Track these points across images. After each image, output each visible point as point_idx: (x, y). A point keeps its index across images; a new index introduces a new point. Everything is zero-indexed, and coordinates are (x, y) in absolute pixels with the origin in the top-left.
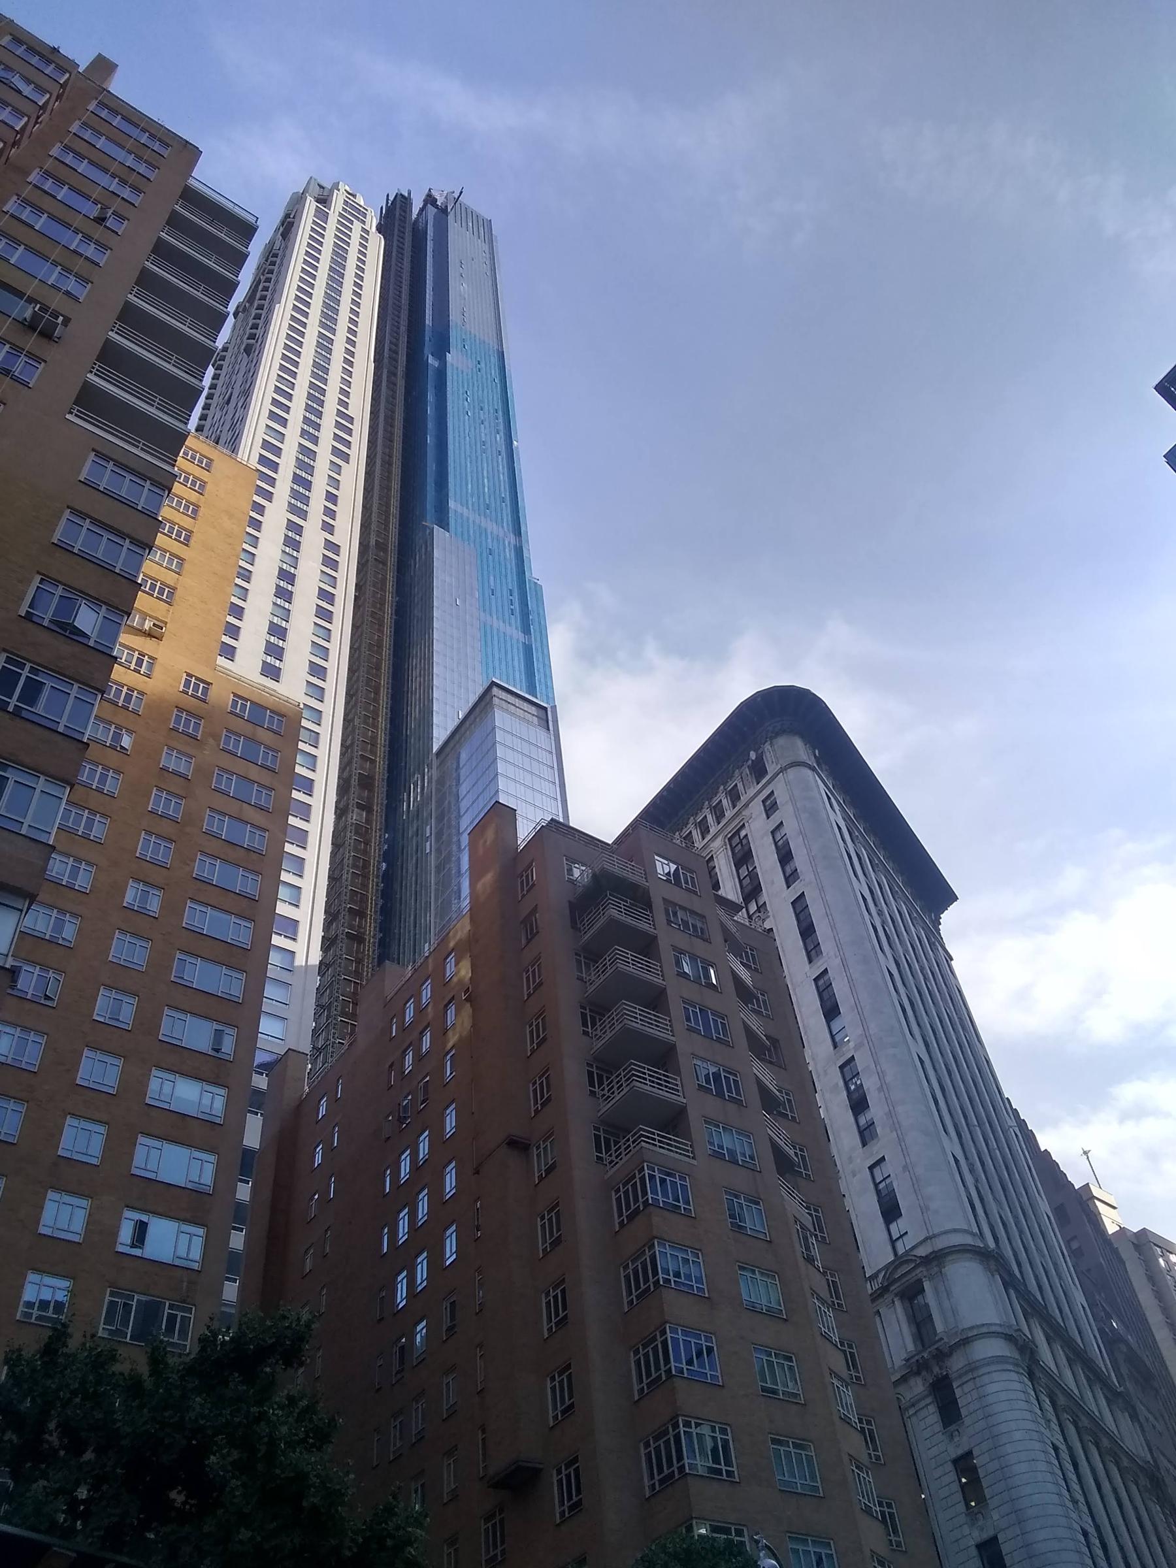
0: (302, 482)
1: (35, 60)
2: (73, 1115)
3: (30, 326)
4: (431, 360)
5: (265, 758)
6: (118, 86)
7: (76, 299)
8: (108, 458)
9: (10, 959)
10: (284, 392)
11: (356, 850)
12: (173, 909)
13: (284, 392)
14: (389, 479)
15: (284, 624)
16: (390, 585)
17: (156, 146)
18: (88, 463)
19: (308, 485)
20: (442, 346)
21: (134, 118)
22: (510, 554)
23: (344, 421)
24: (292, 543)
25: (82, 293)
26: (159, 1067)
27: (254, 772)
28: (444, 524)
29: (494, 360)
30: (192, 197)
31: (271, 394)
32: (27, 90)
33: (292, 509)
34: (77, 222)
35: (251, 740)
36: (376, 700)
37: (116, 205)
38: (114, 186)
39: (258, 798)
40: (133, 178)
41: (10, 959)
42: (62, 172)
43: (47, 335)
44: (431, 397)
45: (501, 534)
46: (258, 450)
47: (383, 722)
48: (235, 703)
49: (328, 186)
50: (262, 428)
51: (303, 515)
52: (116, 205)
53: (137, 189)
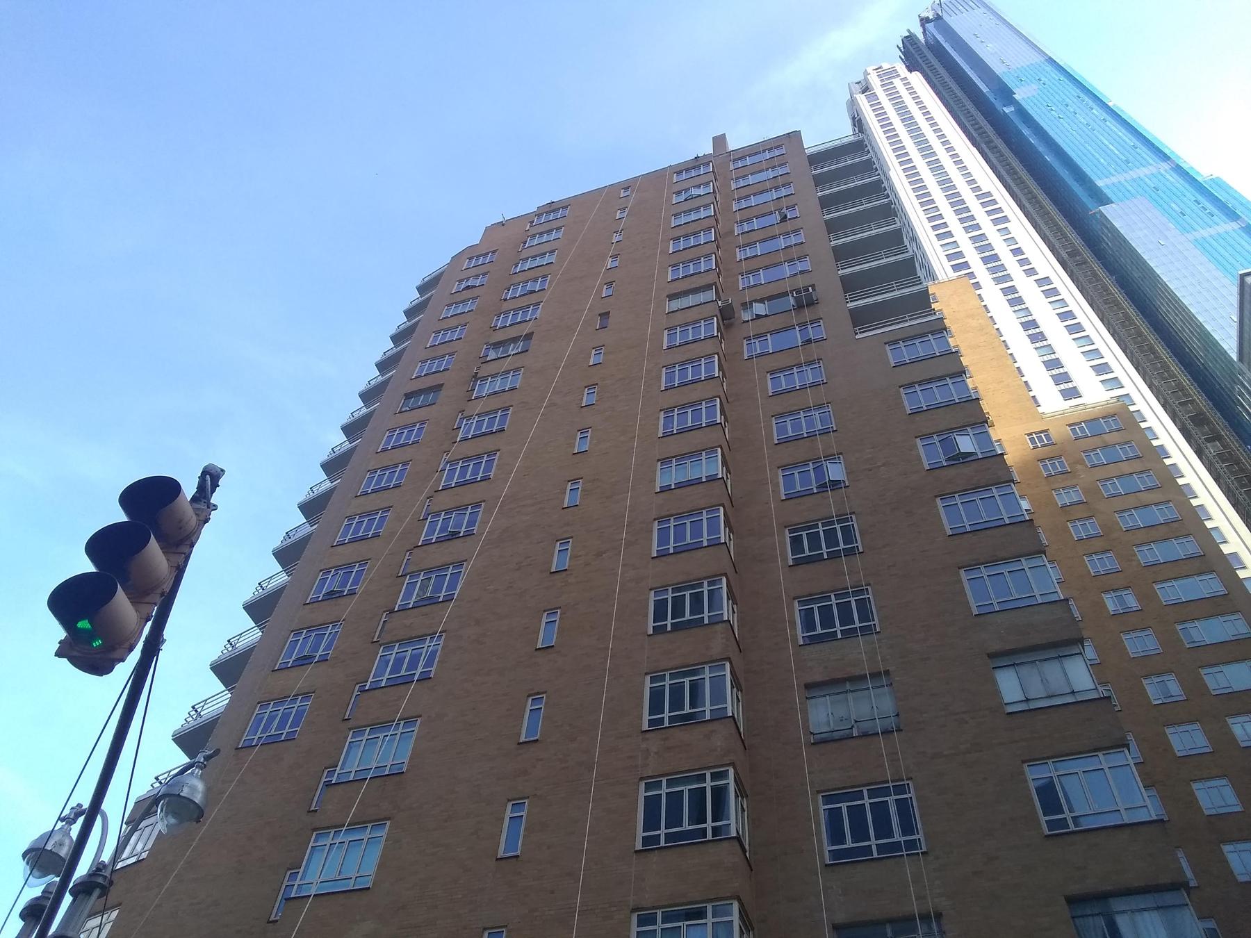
0: (991, 259)
1: (693, 173)
2: (1195, 780)
3: (799, 306)
4: (1007, 110)
5: (1125, 453)
6: (733, 144)
7: (808, 271)
8: (897, 342)
9: (1100, 689)
10: (935, 218)
11: (1233, 473)
12: (1147, 597)
13: (935, 218)
14: (1042, 207)
15: (1053, 357)
16: (1101, 273)
17: (776, 153)
18: (889, 353)
19: (995, 257)
20: (1006, 94)
21: (753, 151)
22: (1173, 178)
23: (986, 200)
24: (1016, 302)
25: (806, 265)
26: (1232, 715)
27: (1126, 468)
28: (1104, 200)
29: (1049, 68)
30: (817, 159)
31: (928, 225)
32: (701, 191)
33: (998, 280)
34: (777, 230)
35: (1105, 447)
36: (1158, 357)
37: (784, 203)
38: (775, 195)
39: (1144, 483)
40: (780, 181)
41: (1100, 689)
42: (746, 214)
43: (811, 303)
44: (1026, 132)
45: (1154, 171)
46: (948, 265)
47: (1175, 368)
48: (1074, 431)
49: (861, 78)
50: (939, 250)
51: (1008, 278)
52: (784, 203)
53: (787, 185)
